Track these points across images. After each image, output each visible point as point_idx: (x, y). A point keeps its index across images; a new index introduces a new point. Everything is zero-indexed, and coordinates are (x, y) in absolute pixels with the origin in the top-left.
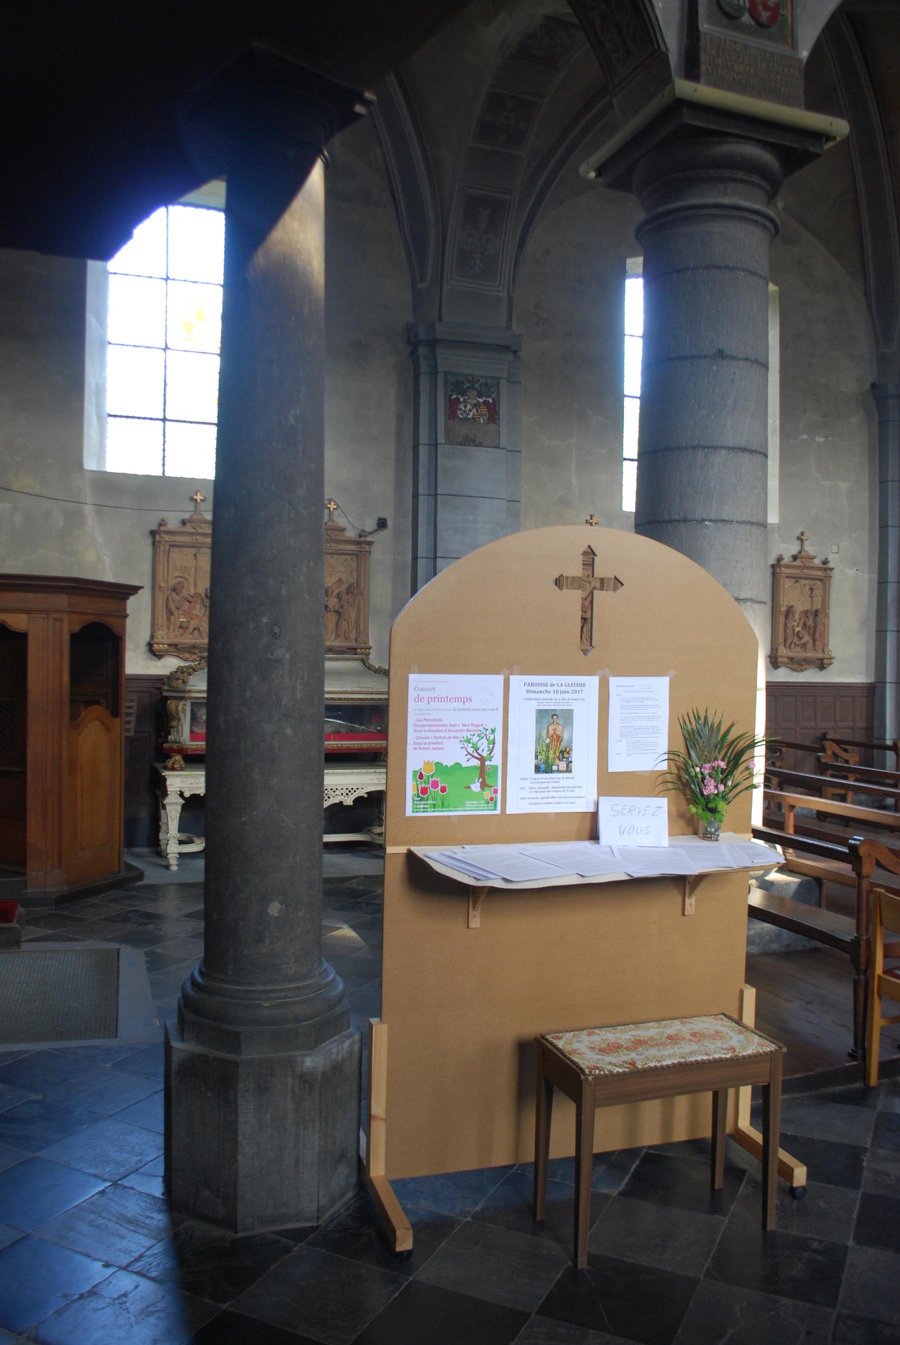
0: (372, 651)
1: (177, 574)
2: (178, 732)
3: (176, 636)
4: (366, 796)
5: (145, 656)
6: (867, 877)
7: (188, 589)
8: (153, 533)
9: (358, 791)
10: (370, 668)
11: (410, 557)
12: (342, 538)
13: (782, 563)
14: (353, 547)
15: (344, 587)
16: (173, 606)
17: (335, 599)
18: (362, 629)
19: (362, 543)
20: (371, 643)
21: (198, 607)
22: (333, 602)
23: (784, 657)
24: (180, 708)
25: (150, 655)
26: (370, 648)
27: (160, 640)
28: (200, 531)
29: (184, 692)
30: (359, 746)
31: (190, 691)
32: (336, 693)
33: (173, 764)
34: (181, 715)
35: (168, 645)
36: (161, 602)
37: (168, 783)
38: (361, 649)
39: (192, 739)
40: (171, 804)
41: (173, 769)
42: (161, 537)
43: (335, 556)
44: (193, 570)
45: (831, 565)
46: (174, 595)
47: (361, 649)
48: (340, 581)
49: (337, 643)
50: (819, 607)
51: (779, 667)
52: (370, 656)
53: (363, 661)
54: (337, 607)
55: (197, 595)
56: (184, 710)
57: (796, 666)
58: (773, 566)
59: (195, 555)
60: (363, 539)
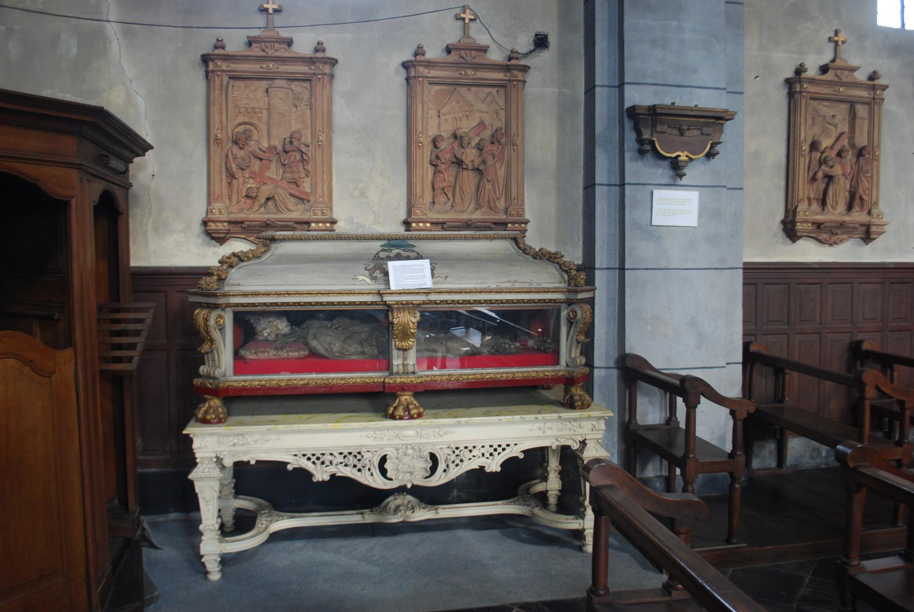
0: (529, 227)
1: (241, 119)
2: (213, 360)
3: (242, 210)
4: (522, 456)
5: (200, 240)
7: (258, 141)
8: (206, 59)
9: (508, 450)
10: (525, 250)
11: (583, 90)
12: (484, 62)
13: (803, 75)
14: (500, 75)
15: (487, 134)
16: (233, 166)
17: (474, 151)
19: (514, 68)
20: (528, 215)
21: (273, 166)
22: (470, 155)
23: (806, 222)
24: (212, 322)
25: (208, 239)
27: (216, 215)
28: (271, 53)
29: (215, 295)
30: (510, 376)
31: (225, 295)
32: (460, 292)
33: (206, 412)
34: (216, 334)
35: (230, 222)
36: (217, 160)
37: (195, 445)
38: (513, 223)
39: (237, 372)
40: (201, 479)
41: (205, 421)
42: (801, 87)
43: (474, 89)
44: (265, 113)
45: (329, 54)
46: (235, 149)
47: (513, 223)
48: (482, 125)
49: (477, 216)
50: (865, 143)
51: (799, 238)
52: (527, 234)
53: (515, 239)
54: (476, 163)
55: (272, 149)
56: (222, 329)
57: (825, 236)
58: (789, 82)
59: (267, 91)
60: (513, 62)
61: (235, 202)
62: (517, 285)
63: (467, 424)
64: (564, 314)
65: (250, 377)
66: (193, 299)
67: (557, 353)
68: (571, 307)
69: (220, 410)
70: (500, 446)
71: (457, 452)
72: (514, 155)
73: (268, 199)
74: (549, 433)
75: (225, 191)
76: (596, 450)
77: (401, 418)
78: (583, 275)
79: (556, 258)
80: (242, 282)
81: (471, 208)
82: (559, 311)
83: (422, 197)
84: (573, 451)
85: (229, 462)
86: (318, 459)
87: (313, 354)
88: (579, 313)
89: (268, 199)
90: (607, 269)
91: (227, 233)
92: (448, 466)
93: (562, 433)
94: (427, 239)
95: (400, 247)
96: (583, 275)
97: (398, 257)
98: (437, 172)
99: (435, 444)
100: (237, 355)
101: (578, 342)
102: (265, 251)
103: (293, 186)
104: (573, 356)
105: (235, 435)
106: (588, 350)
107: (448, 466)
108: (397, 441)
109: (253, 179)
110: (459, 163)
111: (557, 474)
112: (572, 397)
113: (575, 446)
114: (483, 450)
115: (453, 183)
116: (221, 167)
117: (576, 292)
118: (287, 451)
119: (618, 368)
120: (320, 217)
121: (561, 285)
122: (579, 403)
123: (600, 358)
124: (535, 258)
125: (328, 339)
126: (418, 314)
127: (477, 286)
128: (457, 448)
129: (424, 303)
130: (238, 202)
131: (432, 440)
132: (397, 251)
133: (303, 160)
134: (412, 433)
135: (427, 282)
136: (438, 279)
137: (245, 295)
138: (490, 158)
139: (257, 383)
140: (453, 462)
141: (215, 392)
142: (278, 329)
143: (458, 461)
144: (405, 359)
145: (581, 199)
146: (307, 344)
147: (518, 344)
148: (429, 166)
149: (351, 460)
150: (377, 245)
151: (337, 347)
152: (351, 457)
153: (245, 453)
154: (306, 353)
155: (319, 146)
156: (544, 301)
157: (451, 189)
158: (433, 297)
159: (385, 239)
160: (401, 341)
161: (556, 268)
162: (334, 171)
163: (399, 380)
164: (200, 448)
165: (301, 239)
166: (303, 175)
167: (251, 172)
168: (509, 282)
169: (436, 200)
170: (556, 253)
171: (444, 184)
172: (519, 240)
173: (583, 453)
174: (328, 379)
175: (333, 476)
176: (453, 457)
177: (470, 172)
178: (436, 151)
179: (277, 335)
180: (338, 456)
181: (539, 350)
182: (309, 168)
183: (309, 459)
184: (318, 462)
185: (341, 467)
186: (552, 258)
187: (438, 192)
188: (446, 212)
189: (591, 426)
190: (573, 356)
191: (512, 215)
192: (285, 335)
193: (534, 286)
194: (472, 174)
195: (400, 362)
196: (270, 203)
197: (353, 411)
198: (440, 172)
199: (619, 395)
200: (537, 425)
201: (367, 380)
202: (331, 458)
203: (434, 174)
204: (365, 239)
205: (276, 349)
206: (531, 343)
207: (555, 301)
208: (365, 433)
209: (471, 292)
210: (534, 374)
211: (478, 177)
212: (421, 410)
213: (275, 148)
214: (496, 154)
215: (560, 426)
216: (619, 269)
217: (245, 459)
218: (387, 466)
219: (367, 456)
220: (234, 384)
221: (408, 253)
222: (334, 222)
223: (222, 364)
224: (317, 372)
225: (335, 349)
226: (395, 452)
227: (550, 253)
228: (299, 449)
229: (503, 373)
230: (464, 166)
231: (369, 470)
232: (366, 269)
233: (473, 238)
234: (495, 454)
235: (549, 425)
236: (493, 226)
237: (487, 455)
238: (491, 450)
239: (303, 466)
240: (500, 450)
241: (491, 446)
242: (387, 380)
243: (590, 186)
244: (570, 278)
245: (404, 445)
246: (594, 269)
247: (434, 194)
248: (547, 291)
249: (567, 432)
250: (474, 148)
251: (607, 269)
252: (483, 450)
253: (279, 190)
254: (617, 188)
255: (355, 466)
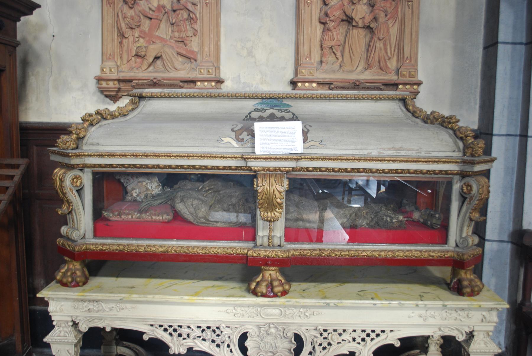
0: (421, 89)
3: (131, 69)
4: (398, 344)
5: (95, 98)
6: (471, 336)
16: (123, 25)
17: (365, 7)
18: (407, 53)
20: (421, 76)
21: (163, 25)
24: (67, 183)
26: (419, 84)
27: (108, 75)
29: (67, 155)
33: (65, 274)
34: (73, 196)
35: (119, 81)
36: (109, 20)
38: (405, 84)
39: (96, 235)
40: (56, 343)
47: (405, 84)
49: (367, 76)
52: (419, 96)
53: (403, 101)
56: (80, 191)
61: (125, 61)
62: (403, 153)
63: (336, 306)
64: (456, 187)
65: (109, 241)
66: (53, 158)
67: (445, 227)
68: (466, 180)
69: (78, 273)
70: (373, 331)
71: (325, 334)
72: (408, 12)
73: (156, 58)
74: (431, 321)
75: (117, 50)
76: (485, 343)
77: (264, 296)
78: (481, 143)
79: (450, 123)
80: (101, 141)
81: (360, 68)
82: (449, 184)
83: (309, 56)
84: (459, 343)
85: (84, 328)
86: (175, 330)
87: (177, 216)
88: (475, 188)
89: (156, 58)
90: (507, 135)
91: (118, 92)
92: (314, 348)
93: (446, 322)
94: (304, 98)
95: (274, 107)
96: (481, 143)
97: (272, 118)
98: (326, 30)
99: (301, 325)
100: (97, 215)
101: (471, 220)
102: (133, 109)
103: (181, 45)
104: (464, 235)
105: (90, 301)
106: (480, 230)
107: (314, 348)
108: (258, 319)
109: (143, 38)
110: (349, 20)
111: (438, 347)
112: (460, 281)
113: (461, 338)
114: (354, 335)
115: (342, 42)
116: (113, 27)
117: (473, 163)
118: (143, 320)
119: (512, 243)
120: (205, 76)
121: (455, 154)
122: (468, 290)
123: (492, 231)
124: (426, 122)
125: (196, 202)
126: (286, 182)
127: (356, 152)
128: (325, 331)
129: (294, 169)
130: (128, 61)
131: (298, 320)
132: (271, 111)
133: (190, 19)
134: (276, 311)
135: (298, 146)
136: (312, 143)
137: (101, 155)
138: (382, 14)
139: (115, 248)
140: (320, 345)
141: (74, 256)
142: (147, 189)
143: (325, 344)
144: (271, 230)
145: (480, 60)
146: (173, 207)
147: (401, 218)
148: (318, 24)
149: (209, 334)
150: (250, 105)
151: (203, 211)
152: (209, 332)
153: (100, 319)
154: (170, 217)
155: (207, 4)
156: (434, 172)
157: (341, 48)
158: (304, 164)
159: (258, 98)
160: (266, 211)
161: (450, 135)
162: (222, 30)
163: (263, 253)
164: (55, 312)
165: (170, 97)
166: (190, 34)
167: (141, 32)
168: (393, 148)
169: (324, 59)
170: (451, 117)
171: (333, 43)
172: (409, 102)
173: (469, 346)
174: (188, 247)
175: (190, 349)
176: (320, 340)
177: (361, 31)
178: (325, 8)
179: (146, 196)
180: (196, 329)
181: (424, 224)
182: (197, 27)
183: (165, 330)
184: (175, 334)
185: (198, 342)
186: (445, 123)
187: (327, 51)
188: (334, 72)
189: (481, 317)
190: (464, 235)
191: (404, 76)
192: (154, 197)
193: (423, 154)
194: (362, 32)
195: (266, 233)
196: (159, 62)
197: (220, 279)
198: (329, 30)
199: (511, 271)
200: (418, 312)
201: (230, 251)
202: (187, 331)
203: (323, 32)
204: (237, 98)
205: (140, 212)
206: (416, 215)
207: (446, 172)
208: (224, 309)
209: (348, 159)
210: (417, 254)
211: (369, 36)
212: (287, 287)
213: (164, 7)
214: (389, 10)
215: (445, 315)
216: (521, 136)
217: (101, 326)
218: (247, 344)
219: (226, 331)
220: (92, 247)
221: (283, 114)
222: (220, 82)
223: (81, 226)
224: (178, 238)
225: (200, 215)
226: (256, 330)
227: (443, 117)
228: (156, 320)
229: (382, 251)
230: (354, 24)
231: (228, 346)
232: (232, 130)
233: (356, 99)
234: (368, 339)
235: (432, 312)
236: (382, 87)
237: (359, 340)
238: (364, 335)
239: (159, 337)
240: (373, 335)
241: (364, 331)
242: (250, 253)
243: (491, 45)
244: (466, 147)
245: (266, 323)
246: (492, 135)
247: (322, 54)
248: (437, 161)
249: (451, 322)
250: (365, 4)
251: (507, 135)
252: (354, 335)
253: (167, 50)
254: (523, 47)
255: (213, 341)
